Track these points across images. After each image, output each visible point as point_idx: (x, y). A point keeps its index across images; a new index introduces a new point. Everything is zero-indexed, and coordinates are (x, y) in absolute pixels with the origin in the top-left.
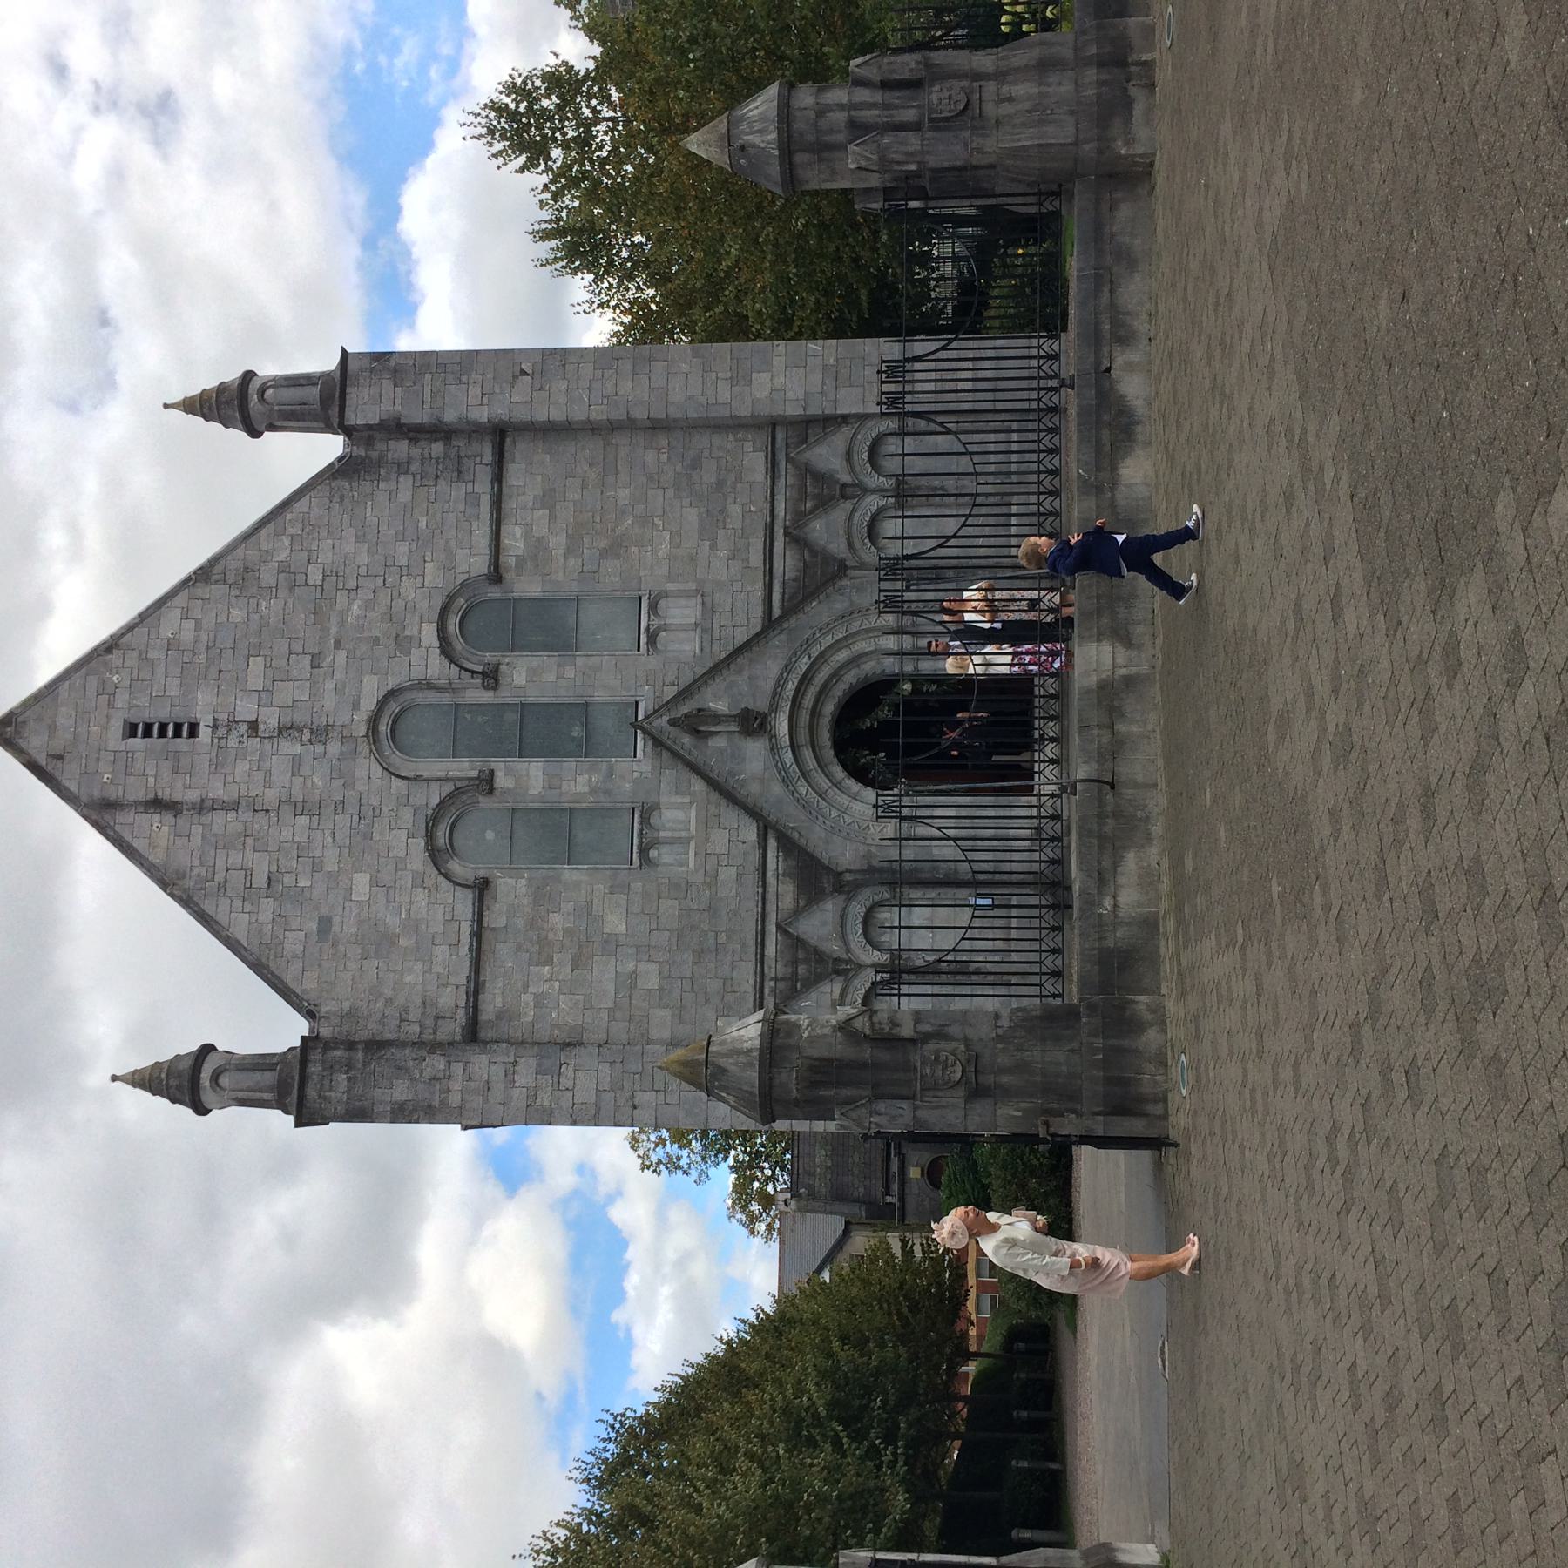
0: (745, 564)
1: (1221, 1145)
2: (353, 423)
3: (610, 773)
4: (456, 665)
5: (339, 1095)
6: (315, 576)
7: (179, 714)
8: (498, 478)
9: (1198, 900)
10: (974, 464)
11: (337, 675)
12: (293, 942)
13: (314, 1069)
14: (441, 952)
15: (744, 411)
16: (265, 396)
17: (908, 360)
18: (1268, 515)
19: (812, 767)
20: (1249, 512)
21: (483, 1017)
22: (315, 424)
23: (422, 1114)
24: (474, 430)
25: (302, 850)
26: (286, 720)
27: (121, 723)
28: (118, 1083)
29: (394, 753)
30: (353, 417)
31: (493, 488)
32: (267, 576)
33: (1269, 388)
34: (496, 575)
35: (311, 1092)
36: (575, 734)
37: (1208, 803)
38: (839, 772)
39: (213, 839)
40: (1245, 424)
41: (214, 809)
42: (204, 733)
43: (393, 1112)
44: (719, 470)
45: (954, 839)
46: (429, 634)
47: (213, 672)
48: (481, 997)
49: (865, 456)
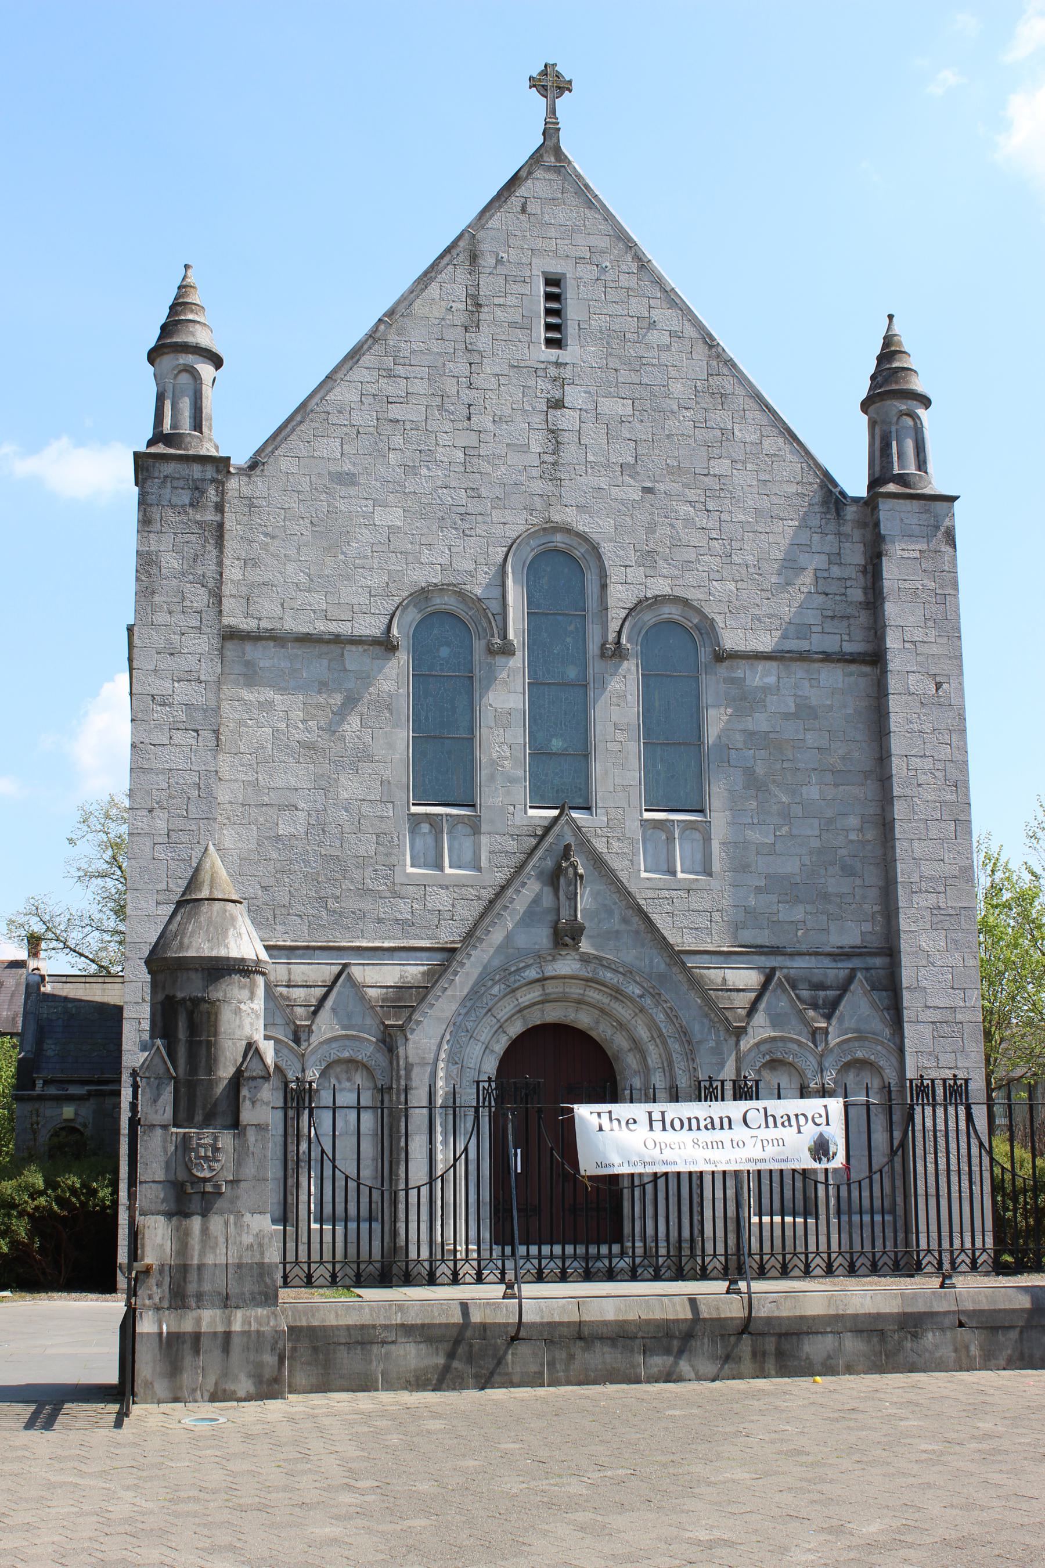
0: (740, 925)
1: (134, 1464)
2: (881, 506)
3: (512, 780)
4: (627, 616)
5: (168, 497)
6: (721, 466)
7: (571, 330)
8: (827, 658)
9: (395, 1436)
10: (860, 1182)
11: (615, 491)
12: (328, 447)
13: (196, 470)
14: (318, 600)
15: (904, 923)
16: (904, 417)
17: (968, 1109)
18: (818, 1507)
19: (520, 1000)
20: (819, 1487)
21: (248, 647)
22: (877, 468)
23: (145, 584)
24: (877, 630)
25: (427, 455)
26: (564, 437)
27: (559, 270)
28: (887, 320)
29: (533, 550)
30: (887, 507)
31: (816, 653)
32: (721, 418)
33: (952, 1506)
34: (721, 657)
35: (169, 468)
36: (554, 741)
37: (502, 1446)
38: (516, 1029)
39: (439, 364)
40: (910, 1480)
41: (470, 364)
42: (553, 354)
43: (148, 553)
44: (841, 896)
45: (454, 1166)
46: (660, 586)
47: (614, 363)
48: (272, 644)
49: (859, 1054)
